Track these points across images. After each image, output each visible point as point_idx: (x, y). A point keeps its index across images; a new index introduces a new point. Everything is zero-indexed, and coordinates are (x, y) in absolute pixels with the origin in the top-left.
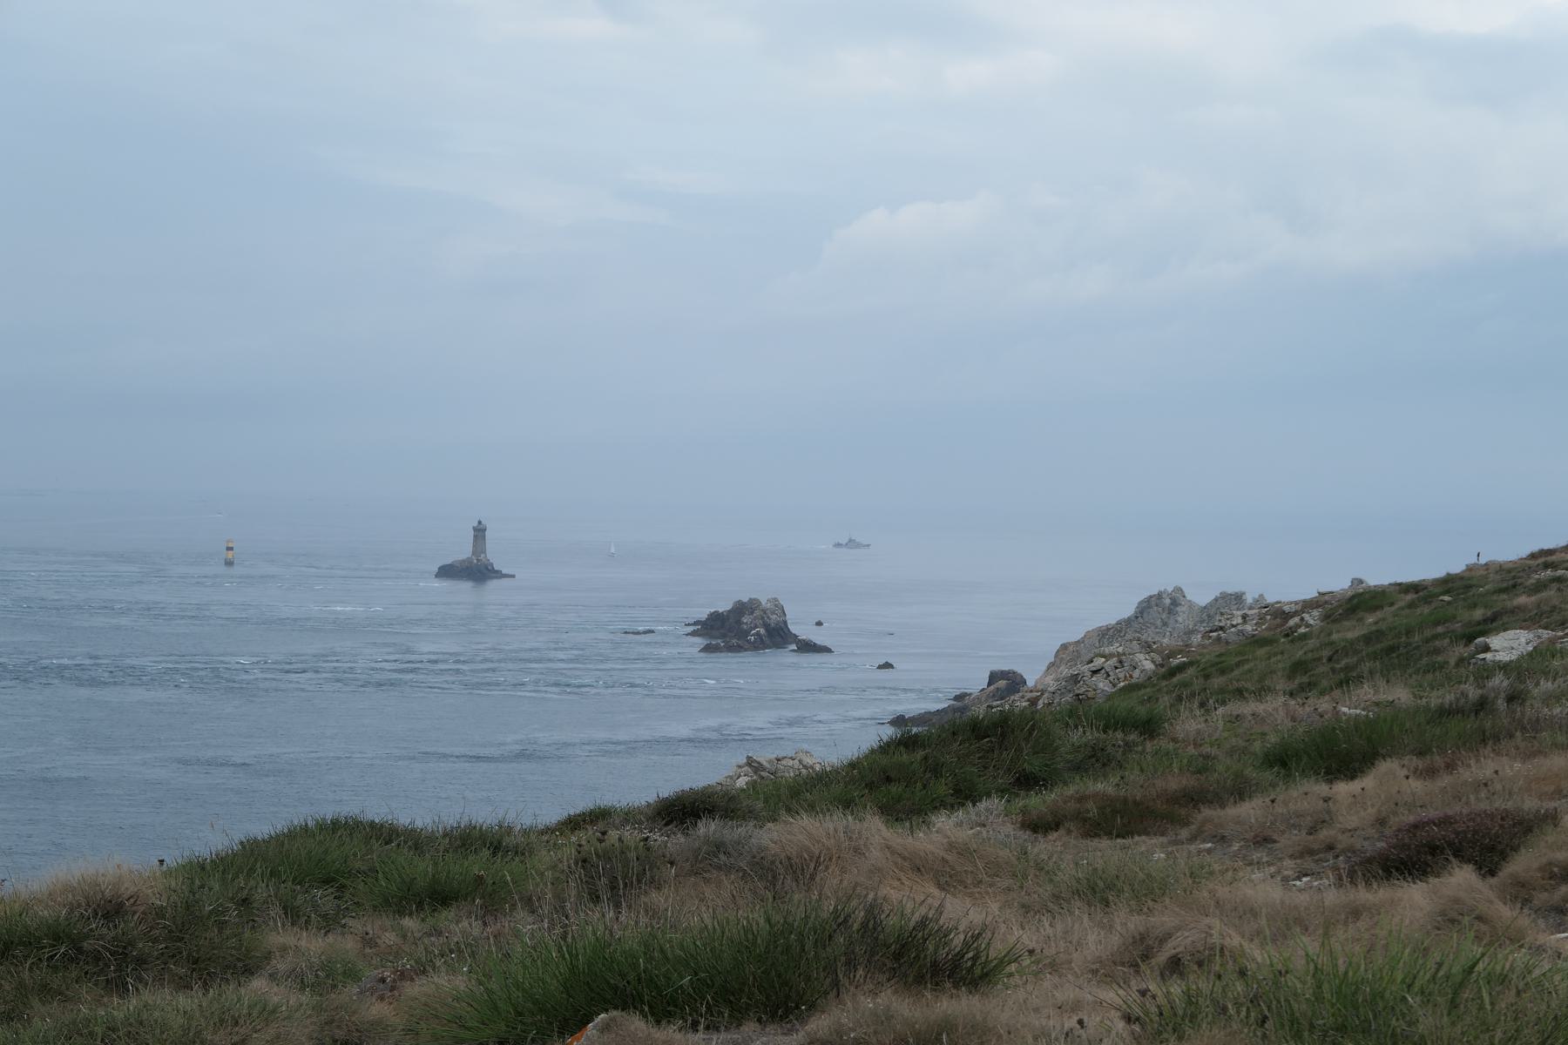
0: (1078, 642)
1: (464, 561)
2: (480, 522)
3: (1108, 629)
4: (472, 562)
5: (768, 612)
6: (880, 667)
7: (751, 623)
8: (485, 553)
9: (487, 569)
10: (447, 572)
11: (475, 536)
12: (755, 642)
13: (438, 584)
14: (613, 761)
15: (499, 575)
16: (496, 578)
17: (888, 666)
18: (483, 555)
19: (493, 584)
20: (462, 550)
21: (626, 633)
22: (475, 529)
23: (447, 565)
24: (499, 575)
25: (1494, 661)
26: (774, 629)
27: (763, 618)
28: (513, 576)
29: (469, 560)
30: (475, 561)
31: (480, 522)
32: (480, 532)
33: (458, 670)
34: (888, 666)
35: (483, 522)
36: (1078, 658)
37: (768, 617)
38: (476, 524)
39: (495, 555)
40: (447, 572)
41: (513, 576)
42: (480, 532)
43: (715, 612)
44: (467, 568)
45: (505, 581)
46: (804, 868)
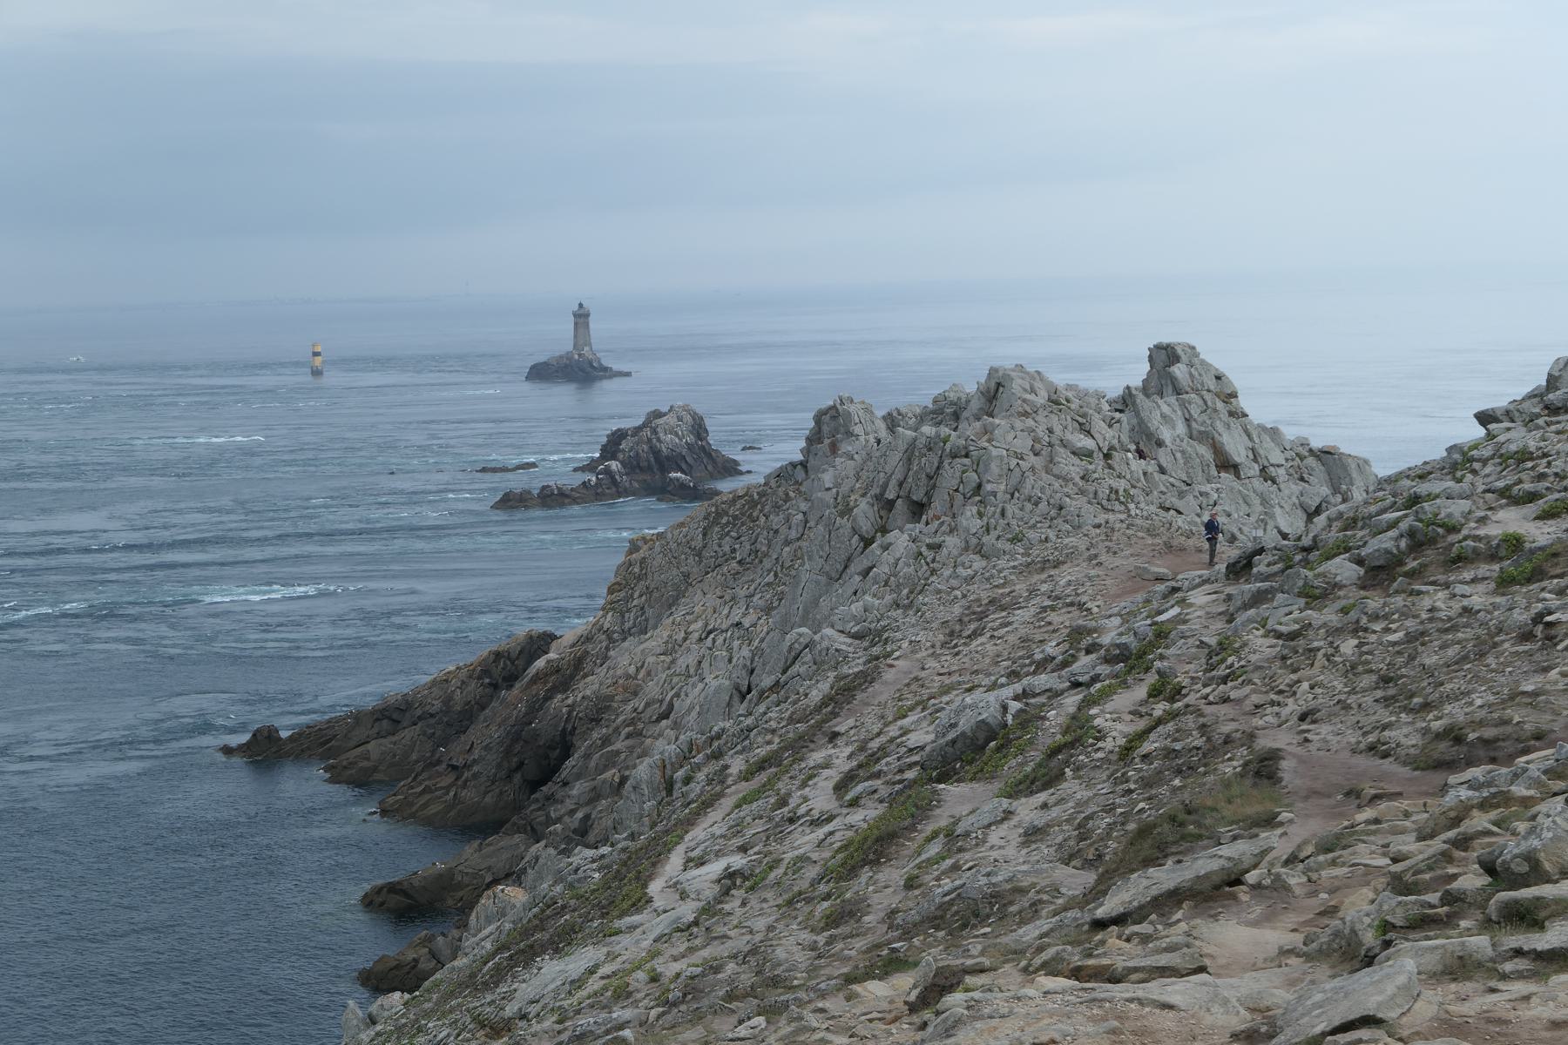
1: (561, 357)
2: (581, 305)
4: (573, 357)
5: (659, 429)
7: (630, 451)
8: (590, 345)
10: (541, 373)
11: (576, 324)
13: (527, 387)
14: (958, 962)
15: (607, 373)
18: (586, 349)
19: (608, 385)
20: (558, 339)
21: (484, 470)
22: (575, 315)
23: (541, 364)
24: (607, 373)
26: (668, 458)
27: (649, 440)
28: (628, 374)
29: (569, 356)
30: (576, 357)
31: (581, 305)
32: (581, 317)
33: (368, 523)
36: (639, 578)
37: (659, 440)
38: (576, 308)
40: (541, 373)
41: (628, 374)
42: (581, 317)
44: (566, 366)
45: (617, 382)
46: (111, 518)
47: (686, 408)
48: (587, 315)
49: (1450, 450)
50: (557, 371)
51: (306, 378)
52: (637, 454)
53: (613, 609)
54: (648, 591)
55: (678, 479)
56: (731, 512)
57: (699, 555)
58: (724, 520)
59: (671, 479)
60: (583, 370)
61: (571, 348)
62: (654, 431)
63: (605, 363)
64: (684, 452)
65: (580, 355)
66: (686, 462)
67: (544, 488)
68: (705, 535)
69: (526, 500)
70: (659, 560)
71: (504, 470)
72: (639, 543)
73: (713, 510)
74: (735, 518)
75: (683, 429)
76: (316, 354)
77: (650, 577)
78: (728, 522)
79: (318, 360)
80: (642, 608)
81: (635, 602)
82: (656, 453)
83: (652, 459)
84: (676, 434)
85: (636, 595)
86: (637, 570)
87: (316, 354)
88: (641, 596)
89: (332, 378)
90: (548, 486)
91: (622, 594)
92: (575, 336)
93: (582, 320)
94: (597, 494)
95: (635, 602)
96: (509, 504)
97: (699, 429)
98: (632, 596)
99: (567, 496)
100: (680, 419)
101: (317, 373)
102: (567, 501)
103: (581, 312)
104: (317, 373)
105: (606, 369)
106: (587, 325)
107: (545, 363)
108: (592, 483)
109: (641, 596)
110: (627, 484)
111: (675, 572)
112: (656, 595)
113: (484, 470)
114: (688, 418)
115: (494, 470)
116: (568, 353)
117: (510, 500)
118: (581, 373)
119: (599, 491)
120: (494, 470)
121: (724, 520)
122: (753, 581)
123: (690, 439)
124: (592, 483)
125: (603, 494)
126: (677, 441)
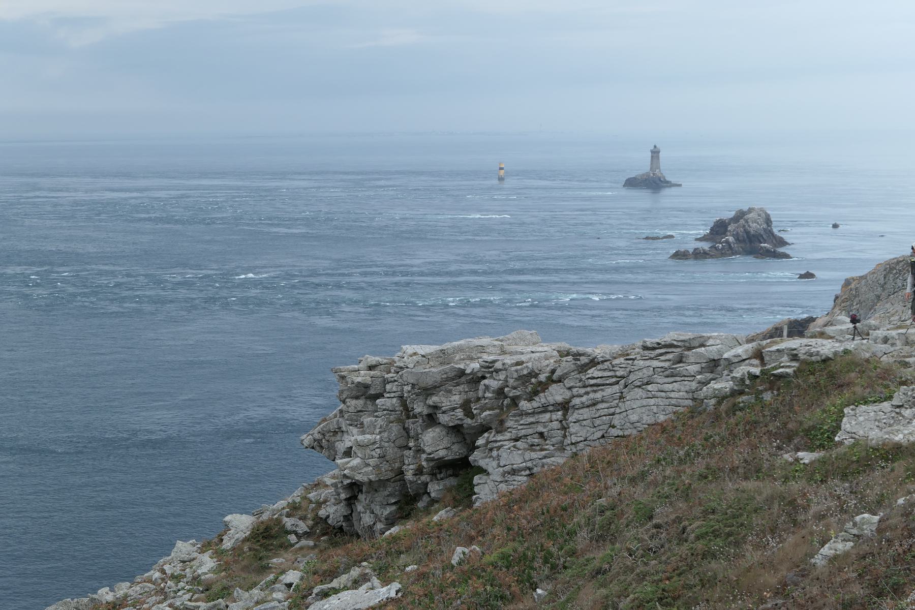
0: (861, 278)
1: (643, 175)
2: (655, 147)
3: (898, 262)
4: (649, 176)
5: (749, 221)
6: (802, 276)
7: (734, 231)
8: (659, 168)
9: (660, 180)
10: (631, 183)
11: (652, 157)
12: (722, 249)
13: (625, 192)
15: (669, 184)
16: (667, 187)
17: (809, 275)
18: (657, 170)
19: (667, 192)
20: (641, 165)
22: (652, 152)
24: (669, 184)
25: (910, 444)
26: (753, 236)
27: (744, 226)
28: (680, 185)
29: (647, 174)
30: (652, 175)
31: (655, 147)
32: (655, 153)
34: (809, 275)
35: (658, 146)
36: (855, 297)
37: (749, 226)
39: (667, 170)
40: (631, 183)
41: (680, 185)
42: (655, 153)
43: (720, 220)
44: (646, 180)
47: (761, 210)
48: (658, 152)
49: (714, 223)
50: (641, 183)
51: (495, 182)
52: (738, 233)
53: (844, 310)
54: (860, 302)
55: (765, 247)
56: (897, 268)
57: (882, 287)
58: (895, 272)
59: (761, 247)
60: (655, 182)
61: (649, 168)
62: (747, 221)
63: (667, 179)
64: (762, 232)
65: (654, 174)
66: (763, 238)
67: (695, 249)
68: (885, 278)
69: (686, 255)
70: (864, 289)
71: (657, 238)
72: (851, 281)
73: (888, 266)
74: (900, 271)
75: (761, 221)
76: (501, 169)
77: (861, 296)
78: (897, 272)
79: (502, 172)
80: (858, 310)
81: (854, 307)
82: (747, 233)
83: (745, 236)
84: (758, 224)
85: (855, 304)
86: (854, 293)
87: (501, 169)
88: (857, 304)
89: (510, 183)
90: (698, 249)
91: (848, 303)
92: (651, 164)
93: (655, 155)
94: (722, 253)
95: (854, 307)
96: (678, 257)
97: (768, 221)
98: (852, 304)
99: (708, 254)
100: (759, 215)
101: (501, 179)
102: (707, 256)
103: (656, 150)
104: (501, 179)
105: (668, 182)
106: (658, 158)
107: (634, 178)
108: (720, 248)
109: (857, 304)
110: (737, 249)
111: (872, 294)
112: (863, 304)
113: (647, 238)
114: (764, 215)
115: (653, 238)
116: (647, 173)
117: (678, 255)
118: (654, 184)
119: (723, 252)
120: (653, 238)
121: (895, 272)
122: (20, 405)
123: (765, 226)
124: (720, 248)
125: (726, 254)
126: (759, 227)
